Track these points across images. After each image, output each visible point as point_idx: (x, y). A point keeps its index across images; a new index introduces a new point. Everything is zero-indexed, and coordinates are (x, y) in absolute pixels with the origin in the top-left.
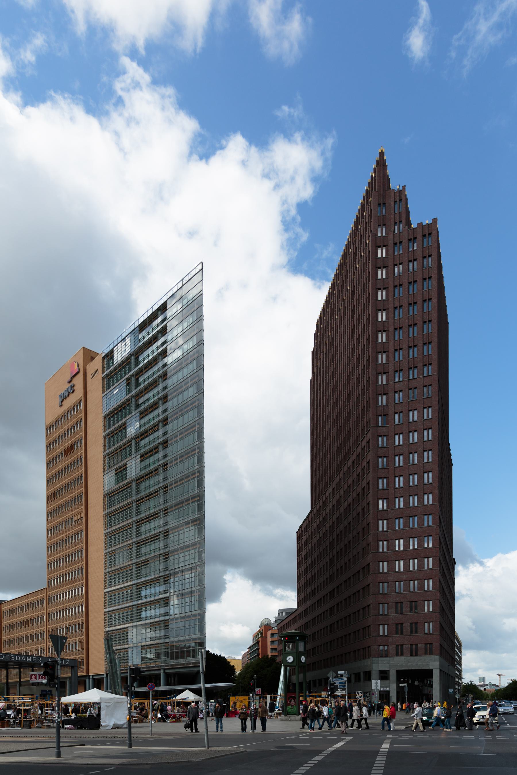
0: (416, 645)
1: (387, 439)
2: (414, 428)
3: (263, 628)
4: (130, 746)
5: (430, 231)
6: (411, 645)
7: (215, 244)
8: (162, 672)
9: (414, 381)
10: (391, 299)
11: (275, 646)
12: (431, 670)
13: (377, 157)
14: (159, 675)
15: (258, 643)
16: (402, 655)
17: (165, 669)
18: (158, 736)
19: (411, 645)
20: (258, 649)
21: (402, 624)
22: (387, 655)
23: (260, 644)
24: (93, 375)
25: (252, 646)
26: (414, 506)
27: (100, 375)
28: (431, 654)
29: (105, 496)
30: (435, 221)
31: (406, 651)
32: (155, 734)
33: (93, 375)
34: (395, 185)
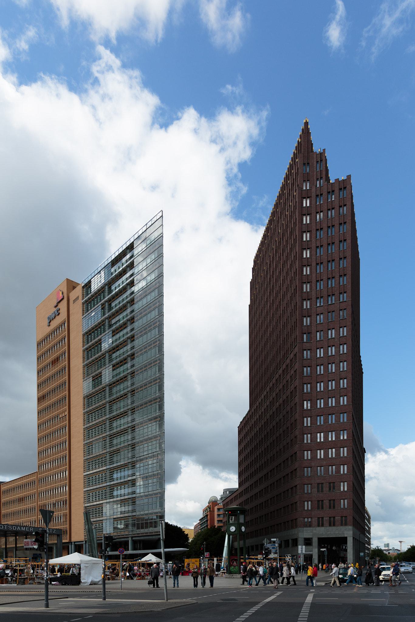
0: (334, 517)
1: (311, 353)
2: (332, 344)
3: (211, 504)
4: (104, 599)
5: (345, 185)
6: (330, 518)
8: (130, 539)
9: (332, 306)
10: (314, 240)
11: (221, 518)
12: (346, 539)
13: (302, 126)
15: (207, 516)
16: (323, 525)
17: (132, 537)
18: (126, 591)
19: (330, 518)
20: (207, 521)
23: (209, 516)
24: (74, 301)
25: (202, 518)
26: (332, 406)
27: (80, 301)
30: (349, 177)
31: (326, 523)
33: (74, 301)
34: (317, 149)
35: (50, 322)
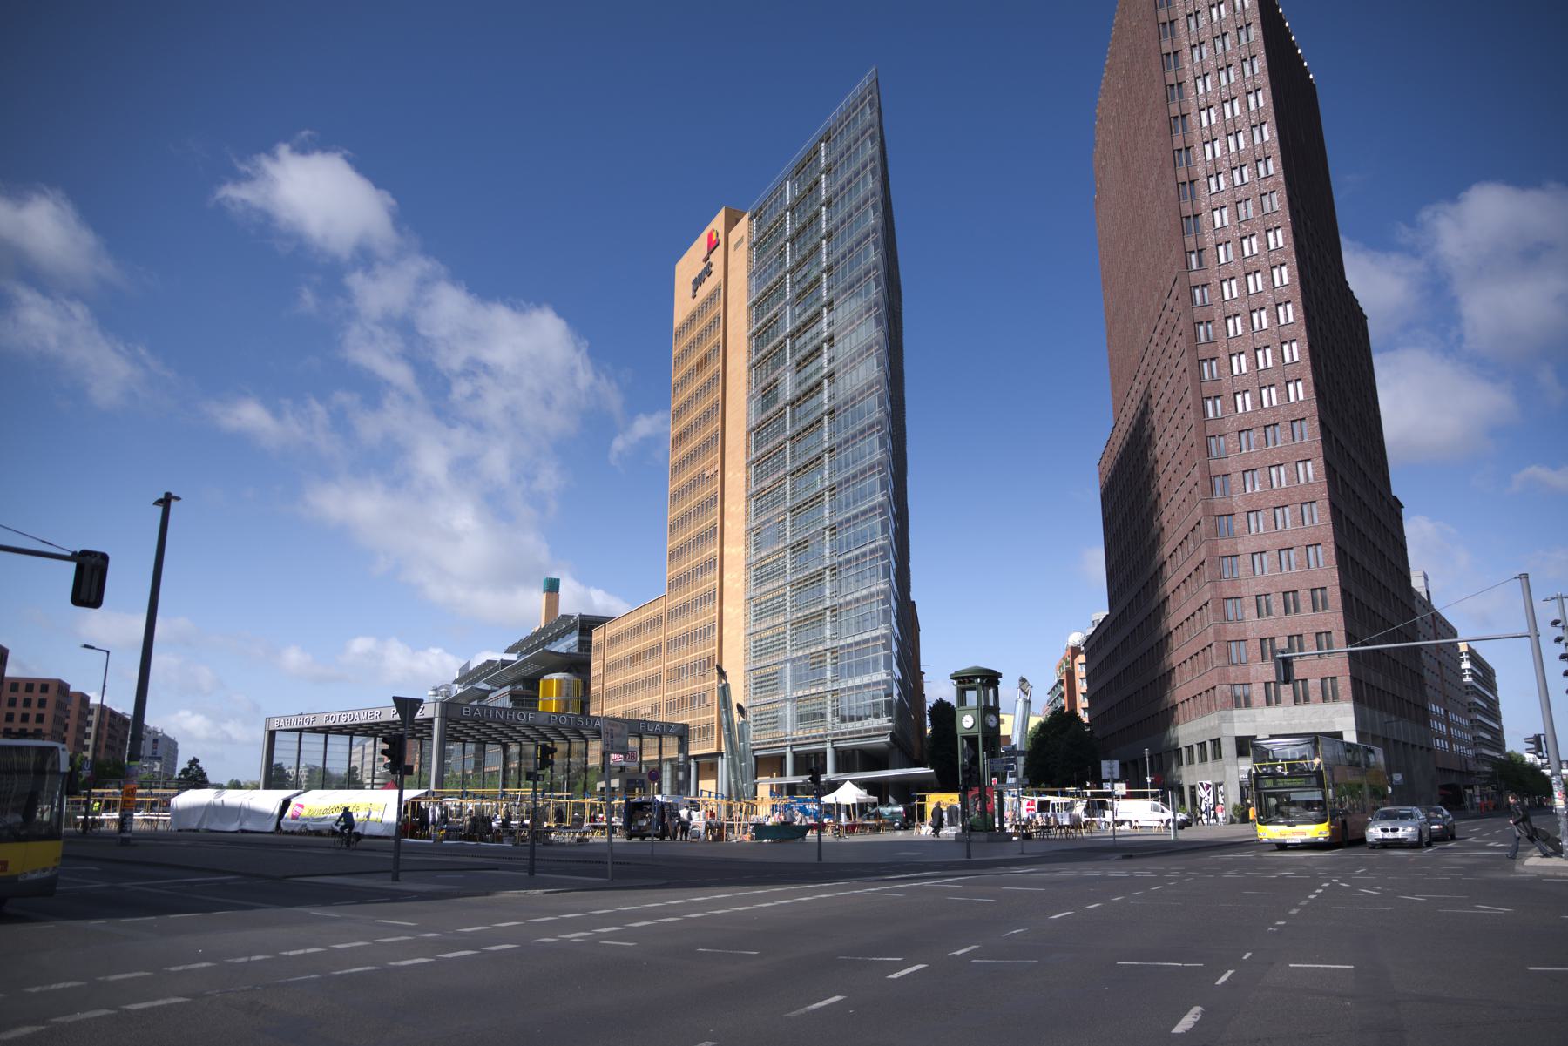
7: (86, 646)
8: (828, 745)
14: (783, 757)
21: (1272, 639)
22: (1248, 704)
24: (736, 246)
28: (1335, 698)
29: (749, 433)
32: (287, 833)
33: (736, 246)
35: (695, 290)
